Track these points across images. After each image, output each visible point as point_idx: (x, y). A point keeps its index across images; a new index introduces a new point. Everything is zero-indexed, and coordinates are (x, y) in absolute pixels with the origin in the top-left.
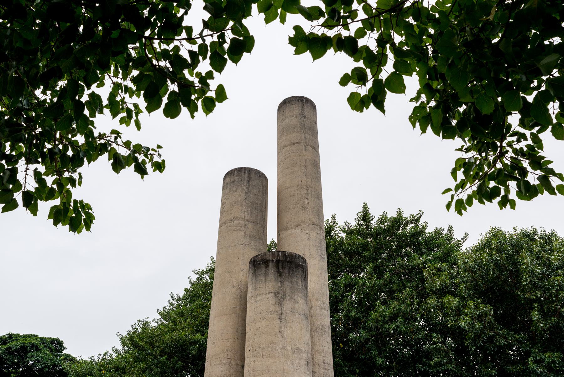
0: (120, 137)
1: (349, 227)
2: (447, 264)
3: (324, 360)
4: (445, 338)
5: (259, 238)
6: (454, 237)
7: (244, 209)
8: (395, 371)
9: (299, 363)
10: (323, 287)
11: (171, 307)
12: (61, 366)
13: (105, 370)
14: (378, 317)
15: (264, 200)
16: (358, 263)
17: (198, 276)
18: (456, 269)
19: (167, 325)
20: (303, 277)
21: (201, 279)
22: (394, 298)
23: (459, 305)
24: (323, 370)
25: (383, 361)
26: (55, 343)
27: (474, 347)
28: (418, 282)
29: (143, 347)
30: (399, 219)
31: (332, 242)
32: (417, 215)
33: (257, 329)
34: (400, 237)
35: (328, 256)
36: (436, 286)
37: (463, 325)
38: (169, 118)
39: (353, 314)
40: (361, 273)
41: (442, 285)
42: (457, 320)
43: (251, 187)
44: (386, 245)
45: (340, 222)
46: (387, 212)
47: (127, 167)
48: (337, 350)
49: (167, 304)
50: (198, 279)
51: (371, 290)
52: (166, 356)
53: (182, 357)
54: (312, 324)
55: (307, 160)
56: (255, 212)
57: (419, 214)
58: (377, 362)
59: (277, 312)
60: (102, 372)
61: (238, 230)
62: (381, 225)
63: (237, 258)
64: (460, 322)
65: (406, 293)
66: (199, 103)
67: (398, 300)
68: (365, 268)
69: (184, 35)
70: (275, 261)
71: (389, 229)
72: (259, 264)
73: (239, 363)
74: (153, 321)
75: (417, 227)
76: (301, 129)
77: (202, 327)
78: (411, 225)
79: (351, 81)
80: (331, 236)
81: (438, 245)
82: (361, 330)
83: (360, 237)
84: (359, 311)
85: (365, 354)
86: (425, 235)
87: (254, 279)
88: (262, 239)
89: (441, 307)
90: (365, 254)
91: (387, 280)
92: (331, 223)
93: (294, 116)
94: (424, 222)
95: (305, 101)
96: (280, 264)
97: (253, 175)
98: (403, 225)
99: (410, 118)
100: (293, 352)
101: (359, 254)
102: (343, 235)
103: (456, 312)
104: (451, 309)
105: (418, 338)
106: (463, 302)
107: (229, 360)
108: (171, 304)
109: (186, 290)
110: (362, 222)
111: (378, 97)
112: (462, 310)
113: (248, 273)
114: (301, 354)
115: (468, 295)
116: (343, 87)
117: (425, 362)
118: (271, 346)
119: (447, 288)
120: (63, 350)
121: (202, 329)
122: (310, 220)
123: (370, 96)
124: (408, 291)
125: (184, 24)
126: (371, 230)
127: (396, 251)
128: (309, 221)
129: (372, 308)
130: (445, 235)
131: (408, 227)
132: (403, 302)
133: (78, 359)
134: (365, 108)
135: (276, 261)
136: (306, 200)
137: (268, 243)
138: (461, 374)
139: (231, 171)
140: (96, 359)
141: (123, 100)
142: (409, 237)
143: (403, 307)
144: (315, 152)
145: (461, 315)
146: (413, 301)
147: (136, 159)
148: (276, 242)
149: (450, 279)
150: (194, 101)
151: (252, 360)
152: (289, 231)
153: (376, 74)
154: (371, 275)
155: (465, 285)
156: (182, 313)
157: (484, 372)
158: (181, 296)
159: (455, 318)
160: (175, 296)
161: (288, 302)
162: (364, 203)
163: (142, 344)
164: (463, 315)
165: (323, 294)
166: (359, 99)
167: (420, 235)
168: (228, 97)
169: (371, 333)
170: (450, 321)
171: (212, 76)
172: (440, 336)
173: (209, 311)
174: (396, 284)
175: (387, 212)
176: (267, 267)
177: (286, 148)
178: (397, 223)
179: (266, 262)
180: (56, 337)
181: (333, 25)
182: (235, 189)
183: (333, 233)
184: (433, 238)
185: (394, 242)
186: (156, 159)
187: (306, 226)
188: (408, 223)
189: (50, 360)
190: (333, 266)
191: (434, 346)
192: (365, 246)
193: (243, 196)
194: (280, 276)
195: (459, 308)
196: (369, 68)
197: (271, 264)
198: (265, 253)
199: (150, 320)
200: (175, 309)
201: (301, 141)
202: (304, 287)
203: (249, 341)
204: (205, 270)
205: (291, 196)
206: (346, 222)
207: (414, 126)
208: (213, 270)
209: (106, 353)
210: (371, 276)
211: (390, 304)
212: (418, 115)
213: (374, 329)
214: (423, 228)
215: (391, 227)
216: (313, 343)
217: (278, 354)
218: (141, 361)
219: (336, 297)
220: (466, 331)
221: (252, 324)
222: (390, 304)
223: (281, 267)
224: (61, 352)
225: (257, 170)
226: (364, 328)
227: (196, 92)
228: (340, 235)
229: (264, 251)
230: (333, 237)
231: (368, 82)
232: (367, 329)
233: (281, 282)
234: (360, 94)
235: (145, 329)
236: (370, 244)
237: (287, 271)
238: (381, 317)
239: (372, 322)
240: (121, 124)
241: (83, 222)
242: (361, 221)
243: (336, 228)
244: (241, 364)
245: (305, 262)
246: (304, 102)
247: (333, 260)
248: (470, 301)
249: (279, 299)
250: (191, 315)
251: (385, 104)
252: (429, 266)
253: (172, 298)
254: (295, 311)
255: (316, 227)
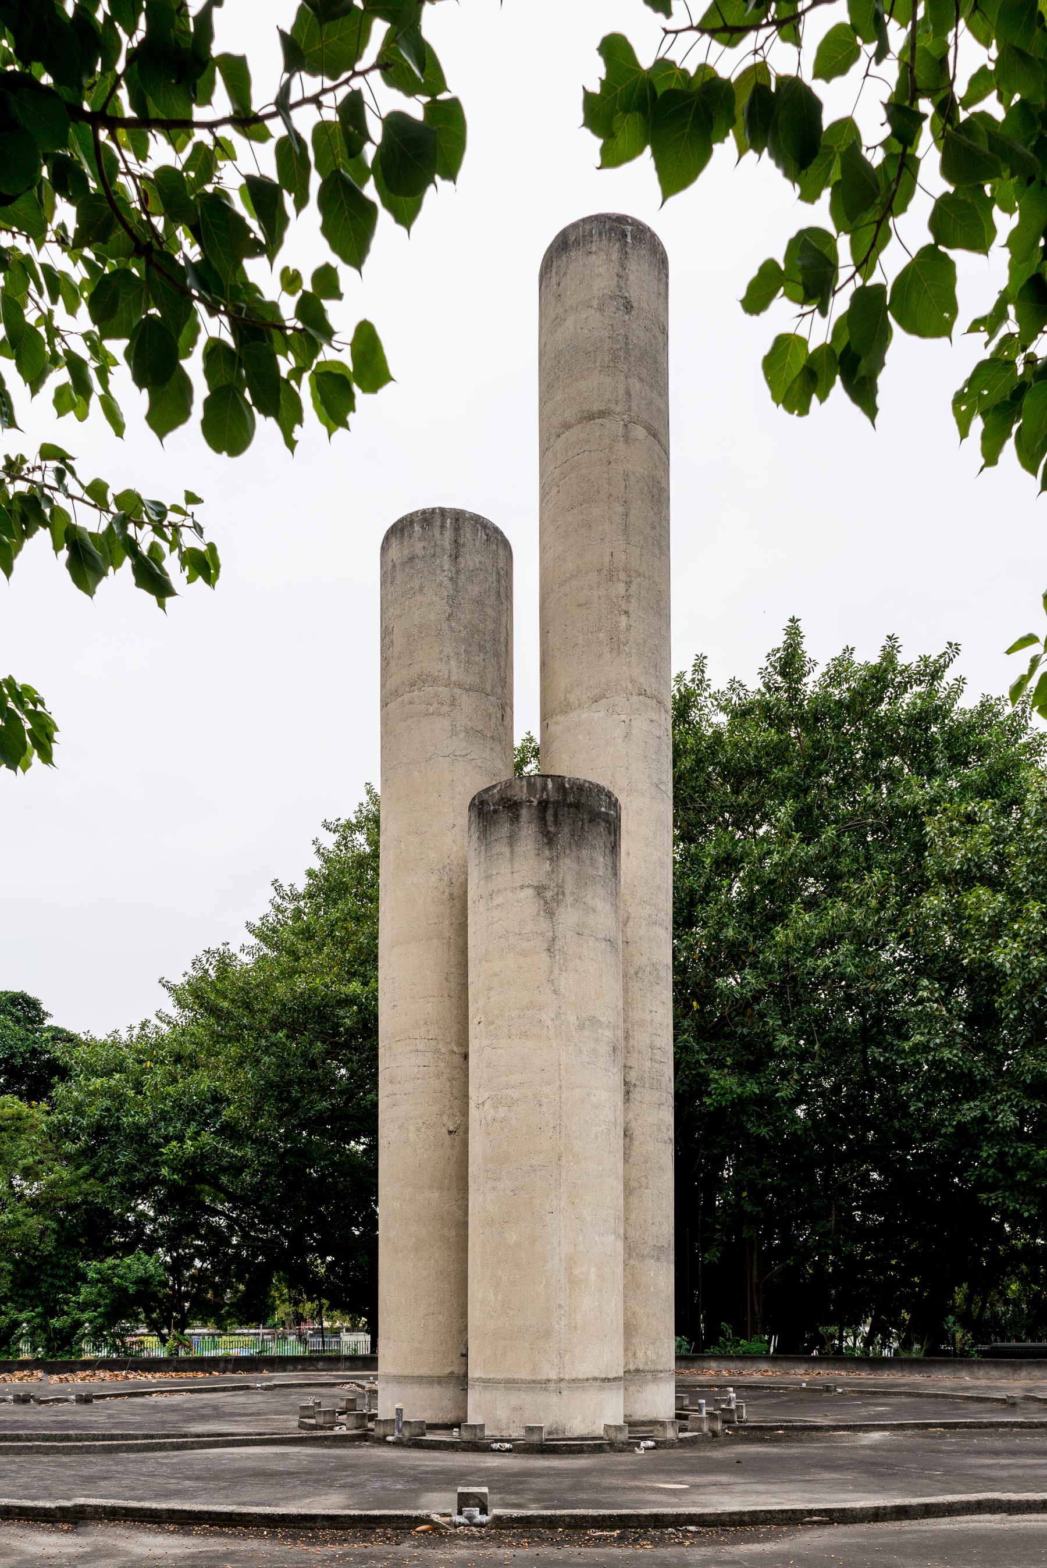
0: (73, 473)
1: (742, 695)
2: (994, 804)
3: (652, 1042)
4: (949, 992)
5: (492, 738)
6: (1031, 724)
7: (449, 650)
8: (817, 1061)
9: (594, 1050)
10: (658, 869)
11: (280, 916)
12: (48, 1052)
13: (151, 1061)
14: (792, 941)
15: (504, 619)
16: (756, 799)
17: (336, 837)
18: (1015, 815)
19: (277, 959)
20: (609, 845)
21: (345, 845)
22: (839, 893)
23: (1002, 911)
24: (649, 1064)
25: (790, 1041)
26: (20, 1004)
27: (1015, 1012)
28: (909, 850)
29: (229, 1013)
30: (885, 670)
31: (691, 740)
32: (940, 657)
33: (495, 975)
34: (879, 726)
35: (678, 780)
36: (951, 864)
37: (1000, 960)
38: (225, 454)
39: (730, 932)
40: (760, 826)
41: (970, 859)
42: (989, 948)
43: (462, 576)
44: (839, 749)
45: (718, 681)
46: (852, 649)
47: (111, 569)
48: (684, 1017)
49: (269, 909)
50: (338, 845)
51: (783, 872)
52: (285, 1031)
53: (322, 1032)
54: (627, 961)
55: (632, 477)
56: (477, 659)
57: (944, 654)
58: (777, 1043)
59: (542, 934)
60: (144, 1065)
61: (432, 714)
62: (830, 689)
63: (436, 795)
64: (995, 953)
65: (870, 882)
66: (305, 391)
67: (847, 899)
68: (773, 813)
69: (221, 104)
70: (535, 803)
71: (853, 700)
72: (495, 811)
73: (456, 1049)
74: (242, 950)
75: (931, 694)
76: (615, 359)
77: (361, 964)
78: (916, 689)
79: (782, 290)
80: (689, 723)
81: (981, 748)
82: (747, 970)
83: (770, 725)
84: (747, 924)
85: (749, 1024)
86: (952, 720)
87: (483, 853)
88: (500, 740)
89: (955, 916)
90: (777, 773)
91: (826, 848)
92: (690, 684)
93: (595, 303)
94: (956, 680)
95: (634, 238)
96: (550, 811)
97: (467, 532)
98: (894, 687)
99: (959, 398)
100: (582, 1027)
101: (760, 773)
102: (721, 719)
103: (990, 927)
104: (979, 921)
105: (883, 990)
106: (1013, 903)
107: (433, 1043)
108: (278, 909)
109: (310, 874)
110: (779, 679)
111: (862, 362)
112: (1006, 925)
113: (466, 835)
114: (600, 1031)
115: (1032, 887)
116: (755, 317)
117: (891, 1044)
118: (530, 1013)
119: (979, 867)
120: (44, 1019)
121: (362, 969)
122: (632, 681)
123: (839, 350)
124: (877, 875)
125: (217, 49)
126: (801, 706)
127: (863, 766)
128: (629, 685)
129: (779, 917)
130: (1008, 717)
131: (907, 695)
132: (860, 903)
133: (84, 1038)
134: (815, 398)
135: (540, 803)
136: (624, 618)
137: (517, 743)
138: (970, 1070)
139: (401, 521)
140: (125, 1037)
141: (47, 319)
142: (905, 725)
143: (858, 914)
144: (657, 448)
145: (1000, 937)
146: (886, 898)
147: (131, 547)
148: (538, 741)
149: (995, 843)
150: (287, 382)
151: (485, 1043)
152: (574, 716)
153: (866, 260)
154: (787, 833)
155: (1029, 861)
156: (309, 932)
157: (1025, 1065)
158: (301, 887)
159: (983, 944)
160: (287, 888)
161: (569, 909)
162: (792, 620)
163: (226, 1004)
164: (1007, 936)
165: (659, 887)
166: (803, 361)
167: (936, 719)
168: (393, 372)
169: (770, 976)
170: (970, 951)
171: (336, 288)
172: (937, 986)
173: (376, 923)
174: (848, 856)
175: (852, 649)
176: (515, 819)
177: (567, 434)
178: (878, 682)
179: (511, 806)
180: (19, 991)
181: (741, 24)
182: (416, 583)
183: (694, 714)
184: (972, 728)
185: (859, 740)
186: (189, 540)
187: (620, 699)
188: (909, 682)
189: (21, 1040)
190: (689, 809)
191: (920, 1008)
192: (779, 753)
193: (442, 606)
194: (548, 844)
195: (1001, 921)
196: (846, 233)
197: (524, 812)
198: (510, 780)
199: (234, 949)
200: (290, 922)
201: (613, 406)
202: (610, 871)
203: (477, 1002)
204: (354, 821)
205: (580, 605)
206: (733, 681)
207: (964, 433)
208: (377, 821)
209: (144, 1025)
210: (787, 835)
211: (825, 908)
212: (986, 392)
213: (779, 968)
214: (948, 696)
215: (857, 695)
216: (627, 1005)
217: (545, 1030)
218: (229, 1042)
219: (692, 892)
220: (1005, 974)
221: (484, 963)
222: (825, 908)
223: (552, 819)
224: (41, 1022)
225: (479, 517)
226: (753, 966)
227: (288, 344)
228: (714, 720)
229: (506, 774)
230: (694, 727)
231: (837, 295)
232: (762, 969)
233: (551, 859)
234: (804, 342)
235: (226, 971)
236: (794, 745)
237: (566, 830)
238: (800, 939)
239: (775, 953)
240: (61, 414)
241: (28, 739)
242: (775, 677)
243: (703, 699)
244: (462, 1050)
245: (614, 804)
246: (629, 240)
247: (689, 790)
248: (1032, 902)
249: (546, 903)
250: (331, 934)
251: (883, 380)
252: (945, 809)
253: (278, 894)
254: (586, 932)
255: (648, 701)
